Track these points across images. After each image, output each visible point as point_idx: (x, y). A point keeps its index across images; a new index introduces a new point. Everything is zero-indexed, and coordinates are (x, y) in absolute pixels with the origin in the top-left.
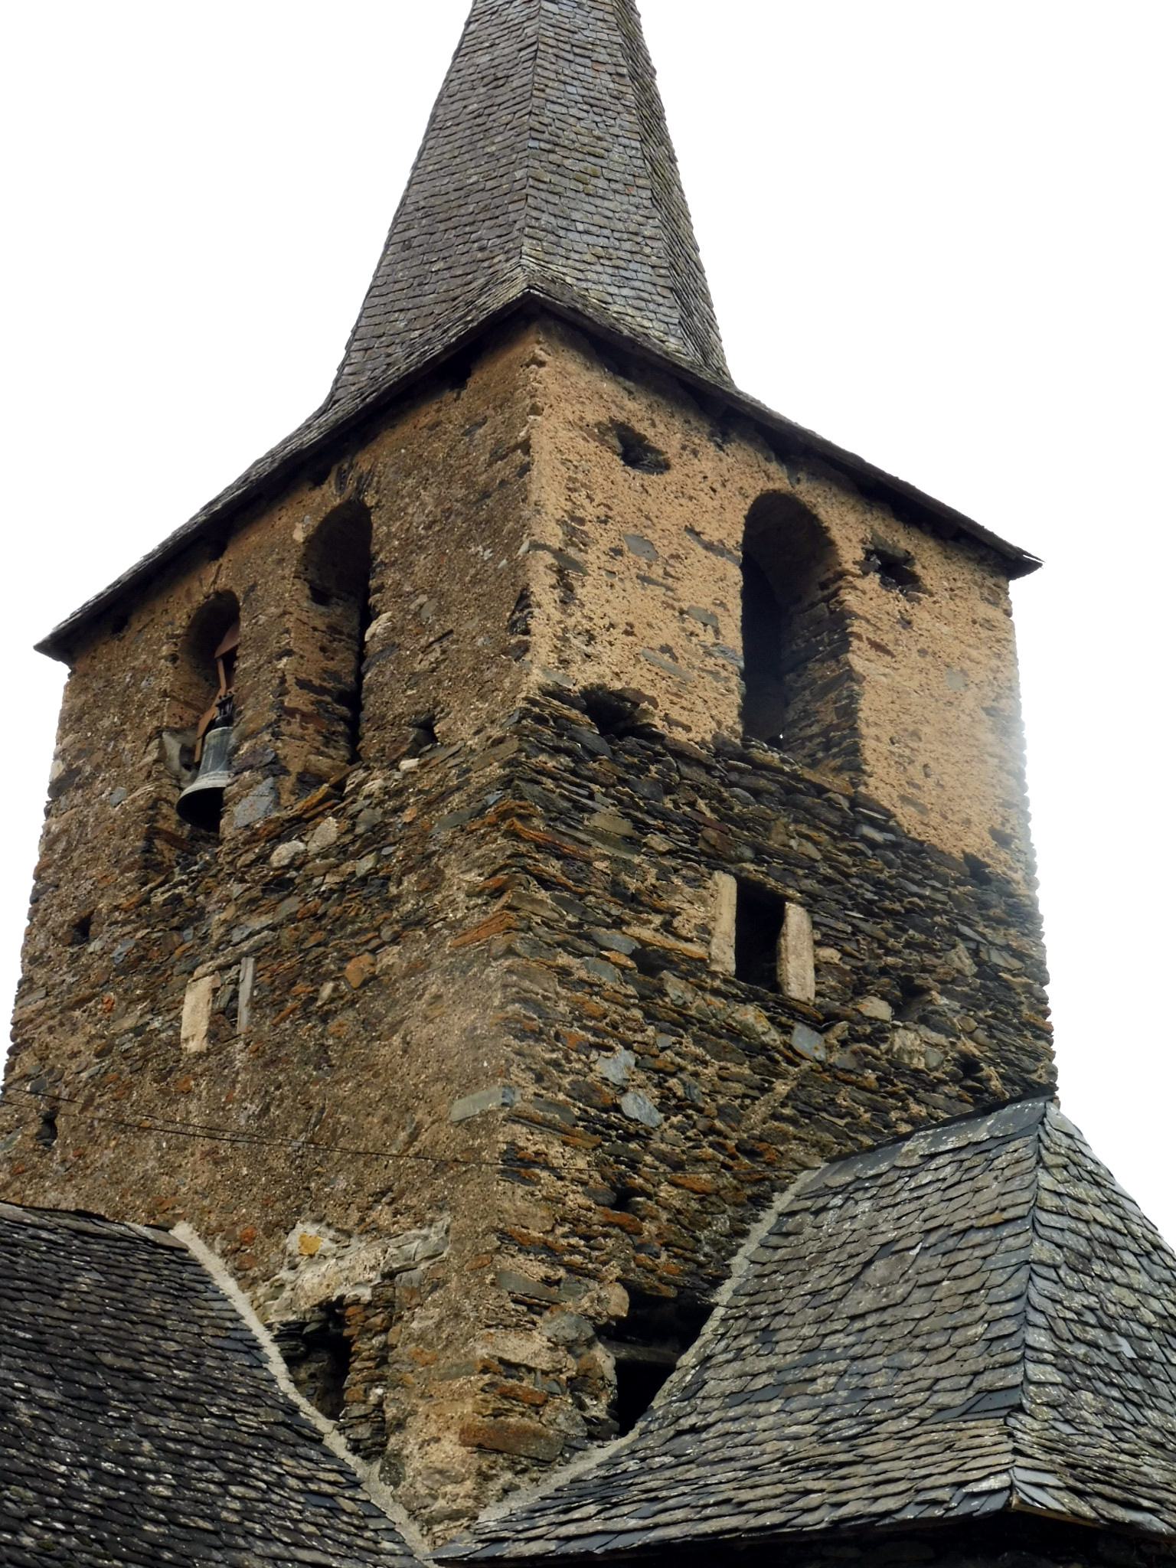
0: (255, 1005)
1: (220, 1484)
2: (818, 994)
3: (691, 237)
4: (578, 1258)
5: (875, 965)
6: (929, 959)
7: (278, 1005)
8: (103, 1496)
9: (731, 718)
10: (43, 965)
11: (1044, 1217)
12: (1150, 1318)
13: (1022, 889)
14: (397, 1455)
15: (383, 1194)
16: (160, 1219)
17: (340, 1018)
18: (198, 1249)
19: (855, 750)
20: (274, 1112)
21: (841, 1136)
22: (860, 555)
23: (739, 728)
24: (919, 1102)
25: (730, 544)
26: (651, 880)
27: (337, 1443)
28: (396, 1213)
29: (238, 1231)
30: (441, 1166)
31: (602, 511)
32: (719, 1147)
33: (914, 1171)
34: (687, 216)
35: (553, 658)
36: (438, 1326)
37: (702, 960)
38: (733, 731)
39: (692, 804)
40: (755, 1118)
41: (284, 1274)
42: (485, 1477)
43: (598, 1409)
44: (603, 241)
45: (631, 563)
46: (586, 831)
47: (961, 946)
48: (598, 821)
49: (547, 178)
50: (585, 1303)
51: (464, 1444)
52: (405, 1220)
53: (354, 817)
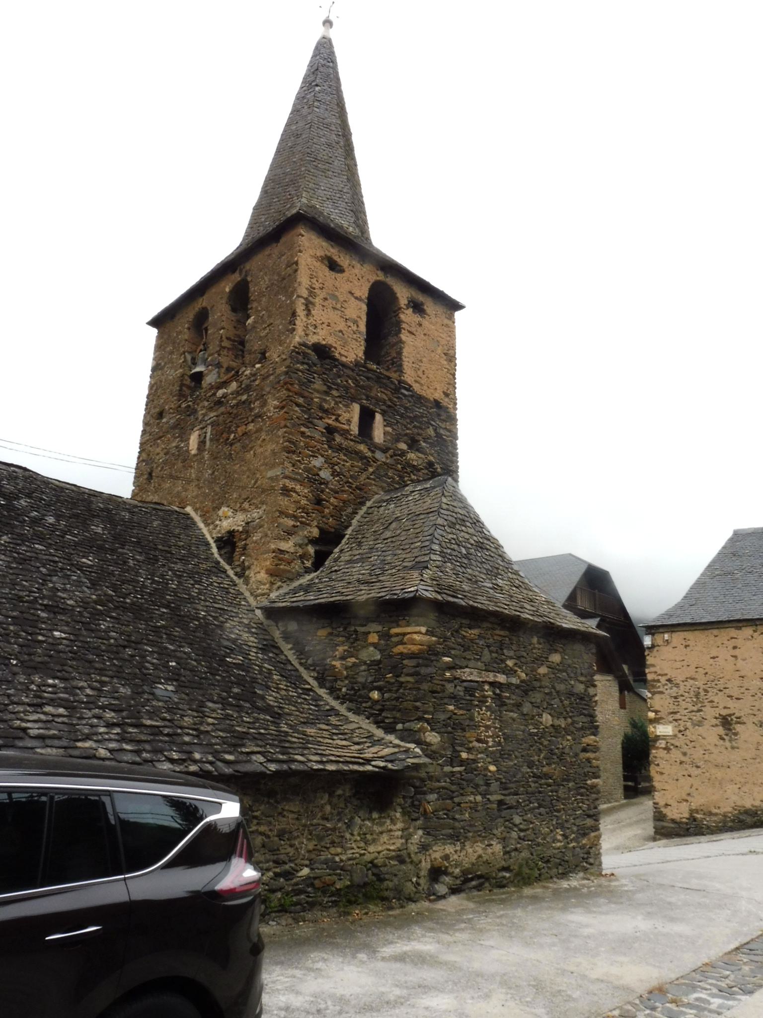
0: (211, 440)
1: (192, 584)
2: (384, 441)
3: (361, 192)
4: (304, 519)
5: (403, 433)
6: (420, 431)
7: (218, 440)
8: (154, 588)
9: (361, 354)
10: (149, 425)
11: (442, 511)
12: (473, 542)
13: (452, 410)
14: (248, 577)
15: (247, 499)
16: (182, 505)
17: (236, 445)
18: (193, 514)
19: (401, 365)
20: (216, 473)
21: (389, 484)
22: (406, 302)
23: (363, 357)
24: (414, 475)
25: (363, 297)
26: (332, 405)
27: (231, 573)
28: (250, 505)
29: (205, 509)
30: (263, 491)
31: (321, 285)
32: (350, 487)
33: (407, 496)
34: (359, 185)
35: (303, 333)
36: (261, 539)
37: (347, 430)
38: (361, 358)
39: (347, 381)
40: (362, 479)
41: (218, 522)
42: (272, 584)
43: (308, 564)
44: (330, 193)
45: (330, 302)
46: (312, 389)
47: (431, 428)
48: (316, 386)
49: (312, 170)
50: (306, 533)
51: (267, 574)
52: (253, 507)
53: (241, 382)
